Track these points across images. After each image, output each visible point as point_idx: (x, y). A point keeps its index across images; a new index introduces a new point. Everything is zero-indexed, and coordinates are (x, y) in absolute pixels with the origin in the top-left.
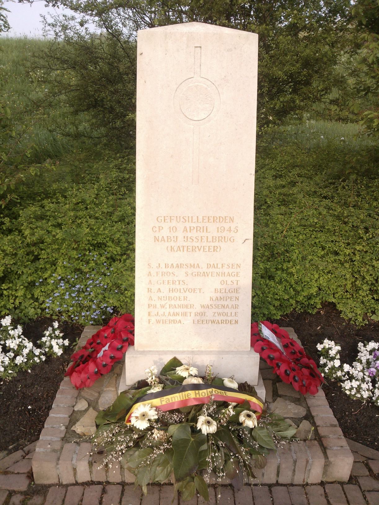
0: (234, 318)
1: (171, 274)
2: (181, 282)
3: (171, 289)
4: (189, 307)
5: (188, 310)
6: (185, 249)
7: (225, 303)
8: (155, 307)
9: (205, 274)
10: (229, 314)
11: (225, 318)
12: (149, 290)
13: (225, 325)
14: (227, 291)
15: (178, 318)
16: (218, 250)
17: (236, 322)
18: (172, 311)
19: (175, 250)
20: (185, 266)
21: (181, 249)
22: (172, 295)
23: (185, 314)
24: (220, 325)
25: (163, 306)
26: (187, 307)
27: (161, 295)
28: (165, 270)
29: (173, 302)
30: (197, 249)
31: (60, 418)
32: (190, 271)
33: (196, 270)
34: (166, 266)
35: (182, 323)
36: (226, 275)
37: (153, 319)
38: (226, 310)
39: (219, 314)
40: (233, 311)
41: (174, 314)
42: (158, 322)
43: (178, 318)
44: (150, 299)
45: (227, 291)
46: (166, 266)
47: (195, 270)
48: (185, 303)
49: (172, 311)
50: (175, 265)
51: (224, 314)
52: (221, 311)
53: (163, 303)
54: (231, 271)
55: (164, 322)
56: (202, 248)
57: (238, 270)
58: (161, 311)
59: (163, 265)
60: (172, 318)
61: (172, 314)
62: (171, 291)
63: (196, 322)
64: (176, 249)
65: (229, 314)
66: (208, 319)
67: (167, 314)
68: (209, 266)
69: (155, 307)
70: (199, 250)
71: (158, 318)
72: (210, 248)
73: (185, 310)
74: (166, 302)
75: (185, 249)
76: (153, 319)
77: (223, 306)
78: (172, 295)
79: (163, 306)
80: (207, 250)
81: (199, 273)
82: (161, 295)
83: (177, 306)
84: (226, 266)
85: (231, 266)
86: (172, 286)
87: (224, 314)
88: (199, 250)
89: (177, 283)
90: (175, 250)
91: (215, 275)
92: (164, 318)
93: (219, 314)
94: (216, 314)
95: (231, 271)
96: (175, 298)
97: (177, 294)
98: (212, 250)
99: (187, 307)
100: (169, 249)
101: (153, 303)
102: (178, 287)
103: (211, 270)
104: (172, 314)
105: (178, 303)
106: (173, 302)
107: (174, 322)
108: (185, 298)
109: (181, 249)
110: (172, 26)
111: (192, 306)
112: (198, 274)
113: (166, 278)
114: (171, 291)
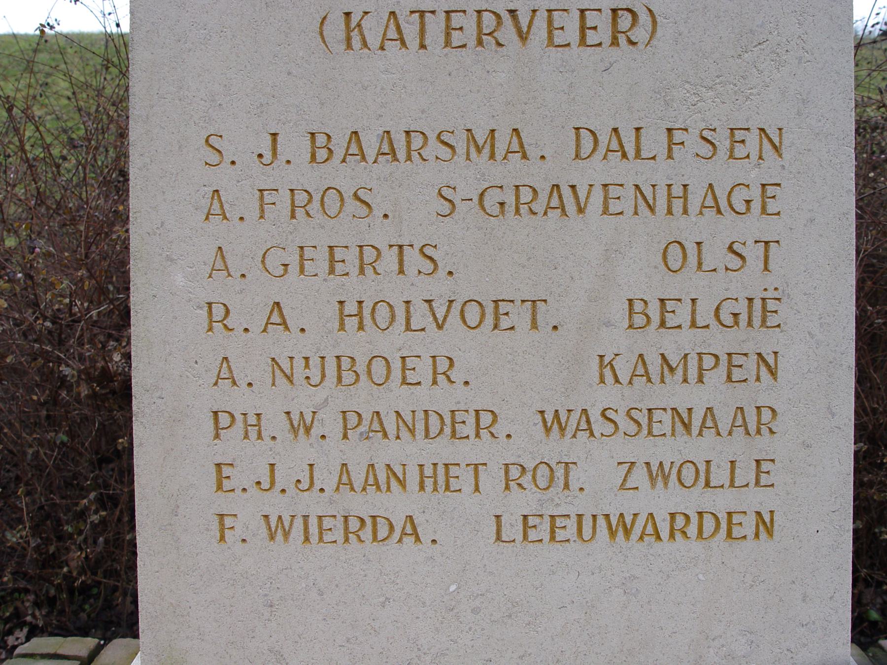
0: (755, 499)
1: (352, 206)
2: (412, 257)
3: (351, 308)
4: (469, 429)
5: (467, 451)
6: (435, 26)
7: (693, 398)
8: (255, 426)
9: (562, 200)
10: (720, 476)
11: (690, 501)
12: (217, 317)
13: (696, 547)
14: (705, 315)
15: (396, 505)
16: (640, 34)
17: (765, 525)
18: (358, 454)
19: (374, 41)
20: (434, 148)
21: (411, 32)
22: (357, 344)
23: (440, 478)
24: (666, 546)
25: (301, 427)
26: (451, 426)
27: (285, 345)
28: (312, 178)
29: (363, 399)
30: (507, 32)
31: (77, 331)
32: (467, 176)
33: (513, 171)
34: (319, 147)
35: (426, 539)
36: (694, 204)
37: (248, 510)
38: (700, 448)
39: (658, 474)
40: (738, 447)
41: (372, 482)
42: (276, 529)
43: (396, 505)
44: (226, 373)
45: (705, 315)
46: (319, 147)
47: (497, 173)
48: (443, 399)
49: (358, 454)
50: (371, 143)
51: (688, 474)
52: (669, 450)
53: (303, 400)
54: (723, 173)
55: (314, 531)
56: (541, 22)
57: (771, 168)
58: (293, 459)
59: (294, 146)
60: (361, 505)
61: (358, 480)
62: (351, 323)
63: (513, 530)
64: (373, 31)
65: (720, 476)
66: (584, 505)
67: (327, 478)
68: (584, 141)
69: (255, 426)
70: (523, 37)
71: (276, 505)
72: (592, 19)
73: (442, 450)
74: (321, 394)
75: (435, 26)
76: (248, 510)
77: (683, 421)
78: (357, 344)
79: (301, 427)
80: (572, 34)
81: (526, 195)
82: (285, 345)
83: (390, 424)
84: (692, 141)
85: (723, 144)
86: (356, 288)
87: (688, 474)
88: (523, 37)
89: (390, 259)
90: (374, 41)
91: (627, 205)
92: (312, 505)
93: (658, 474)
94: (639, 477)
95: (723, 173)
96: (379, 367)
97: (393, 343)
98: (604, 34)
99: (451, 426)
100: (336, 30)
101: (239, 401)
102: (394, 290)
103: (594, 172)
104: (358, 480)
105: (395, 399)
106: (363, 399)
107: (374, 527)
108: (443, 370)
109: (411, 32)
110: (136, 484)
111: (485, 422)
112: (521, 202)
113: (316, 233)
114: (351, 323)
